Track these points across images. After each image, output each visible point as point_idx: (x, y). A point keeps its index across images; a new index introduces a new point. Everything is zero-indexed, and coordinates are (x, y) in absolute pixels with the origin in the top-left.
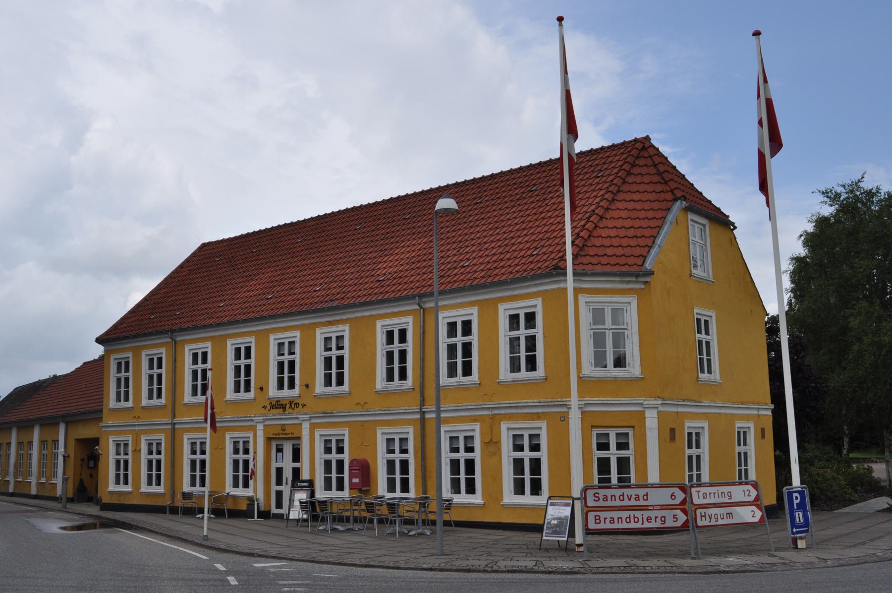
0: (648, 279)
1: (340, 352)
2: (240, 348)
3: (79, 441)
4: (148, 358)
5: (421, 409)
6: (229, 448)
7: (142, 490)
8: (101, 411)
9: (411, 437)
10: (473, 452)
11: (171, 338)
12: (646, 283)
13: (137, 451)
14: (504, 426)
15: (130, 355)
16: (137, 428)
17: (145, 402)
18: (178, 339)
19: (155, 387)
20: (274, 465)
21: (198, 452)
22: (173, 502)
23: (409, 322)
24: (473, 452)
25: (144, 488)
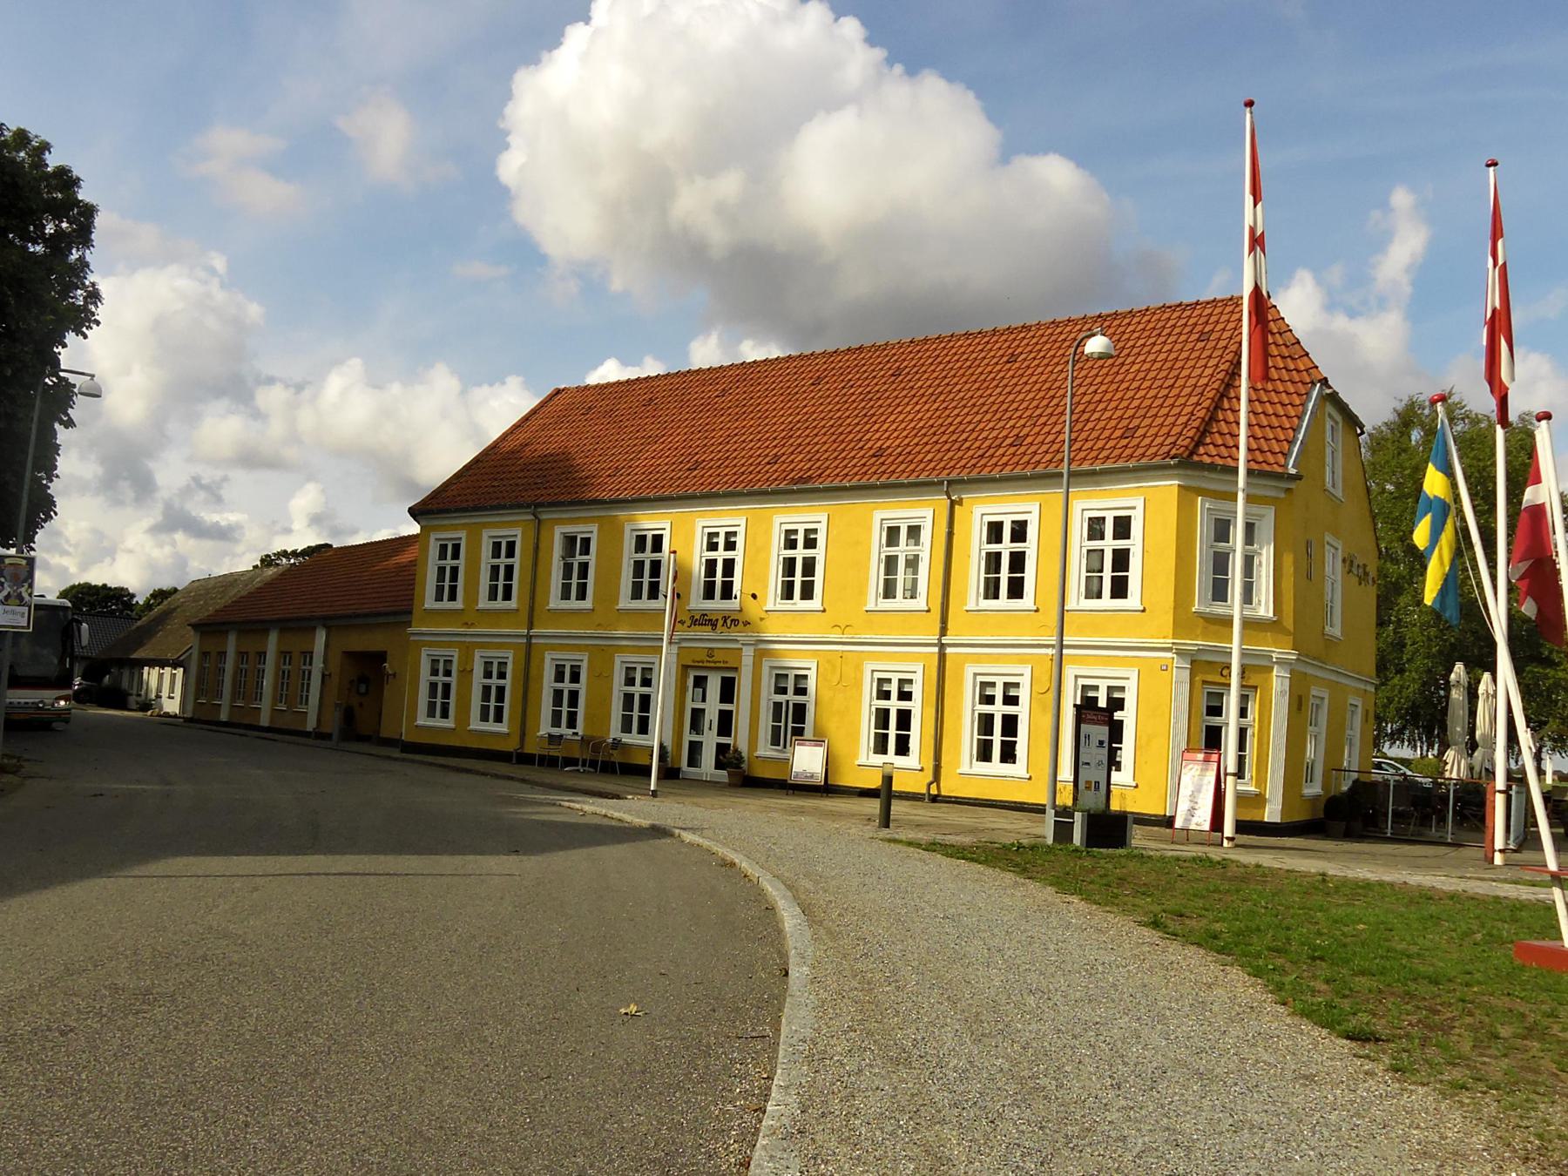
0: (1292, 486)
1: (810, 553)
2: (1001, 523)
3: (351, 656)
4: (491, 541)
5: (940, 640)
6: (619, 677)
7: (420, 722)
8: (410, 613)
9: (918, 678)
10: (1017, 704)
11: (534, 515)
12: (1288, 490)
13: (466, 673)
14: (477, 654)
15: (463, 534)
16: (468, 639)
17: (484, 603)
18: (544, 517)
19: (447, 584)
20: (690, 705)
21: (638, 681)
22: (522, 746)
23: (517, 534)
24: (1017, 704)
25: (476, 724)
